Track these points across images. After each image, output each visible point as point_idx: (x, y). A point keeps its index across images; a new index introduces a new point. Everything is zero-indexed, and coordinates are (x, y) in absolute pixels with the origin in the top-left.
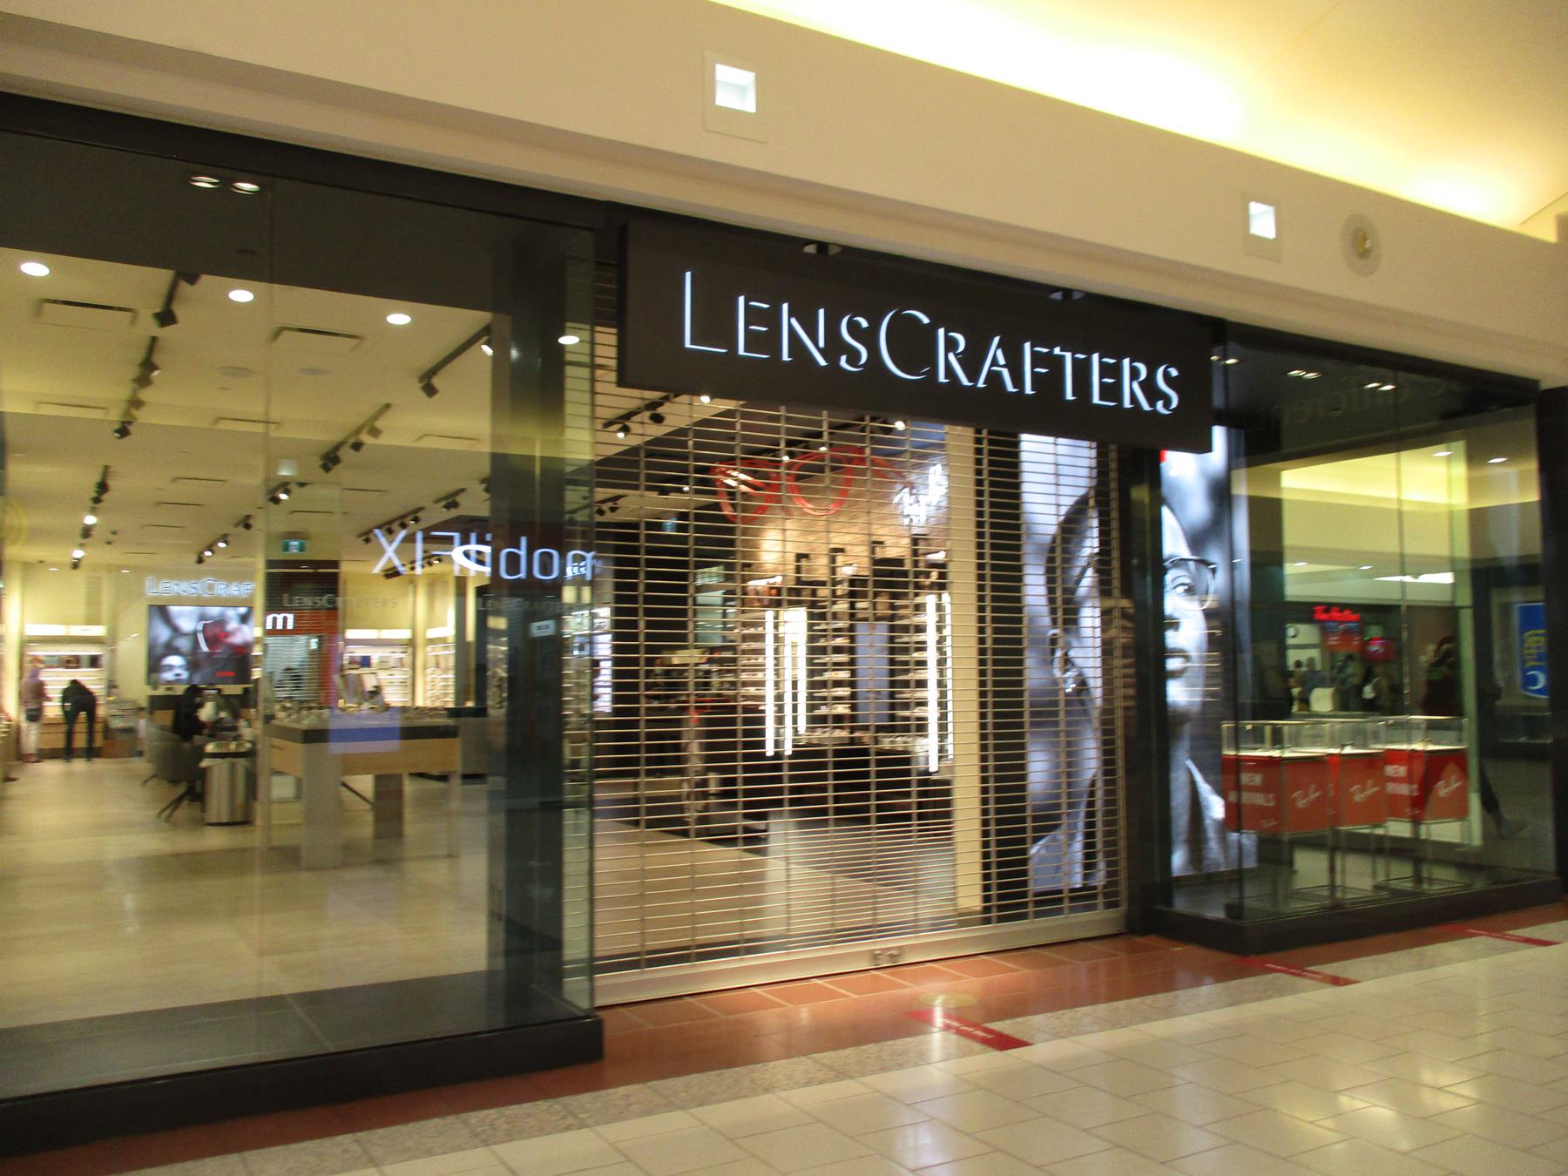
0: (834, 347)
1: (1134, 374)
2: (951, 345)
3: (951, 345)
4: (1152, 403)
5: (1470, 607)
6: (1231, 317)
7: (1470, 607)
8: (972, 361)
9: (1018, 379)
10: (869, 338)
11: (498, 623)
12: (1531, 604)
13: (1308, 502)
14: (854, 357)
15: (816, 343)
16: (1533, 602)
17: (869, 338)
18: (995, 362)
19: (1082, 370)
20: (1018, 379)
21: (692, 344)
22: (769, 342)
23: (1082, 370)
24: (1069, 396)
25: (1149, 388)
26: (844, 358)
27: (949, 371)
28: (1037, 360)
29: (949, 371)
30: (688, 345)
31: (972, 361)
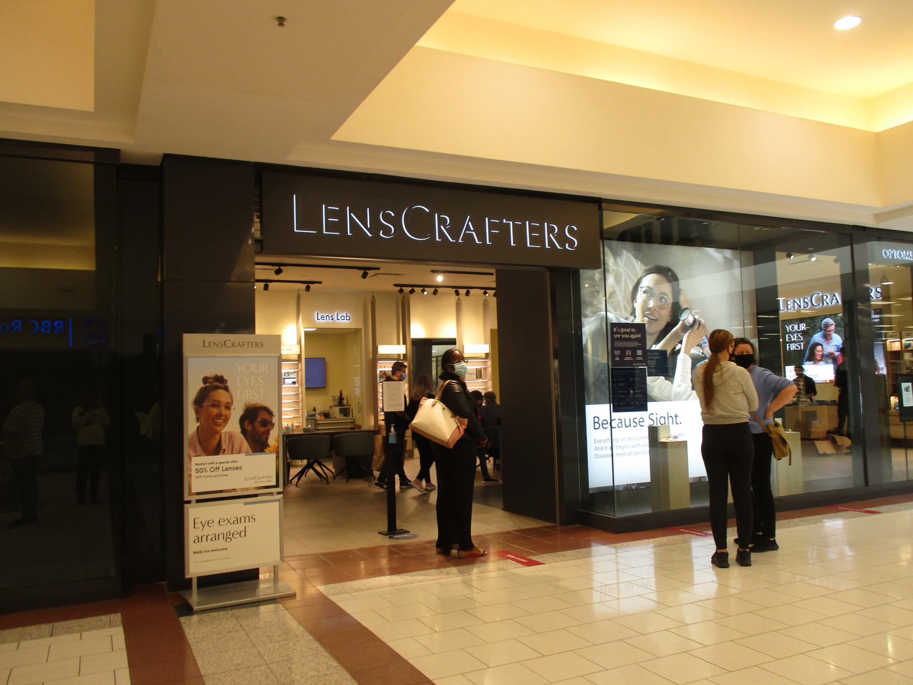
0: (376, 226)
1: (551, 230)
2: (442, 222)
3: (551, 230)
4: (563, 245)
5: (905, 437)
6: (603, 197)
7: (905, 437)
8: (455, 232)
9: (482, 236)
10: (396, 222)
11: (615, 385)
12: (345, 427)
13: (7, 268)
14: (387, 231)
15: (366, 227)
16: (345, 422)
17: (396, 222)
18: (468, 228)
19: (520, 231)
20: (482, 236)
21: (297, 230)
22: (341, 226)
23: (520, 231)
24: (370, 235)
25: (561, 238)
26: (567, 244)
27: (441, 234)
28: (492, 226)
29: (441, 234)
30: (529, 245)
31: (455, 230)
